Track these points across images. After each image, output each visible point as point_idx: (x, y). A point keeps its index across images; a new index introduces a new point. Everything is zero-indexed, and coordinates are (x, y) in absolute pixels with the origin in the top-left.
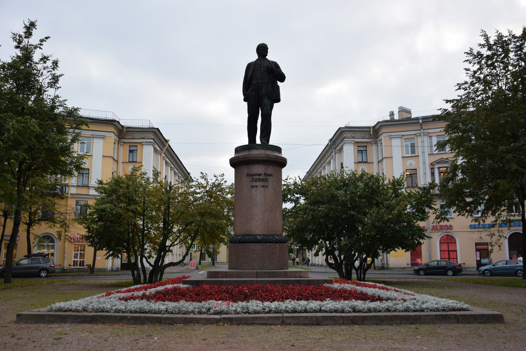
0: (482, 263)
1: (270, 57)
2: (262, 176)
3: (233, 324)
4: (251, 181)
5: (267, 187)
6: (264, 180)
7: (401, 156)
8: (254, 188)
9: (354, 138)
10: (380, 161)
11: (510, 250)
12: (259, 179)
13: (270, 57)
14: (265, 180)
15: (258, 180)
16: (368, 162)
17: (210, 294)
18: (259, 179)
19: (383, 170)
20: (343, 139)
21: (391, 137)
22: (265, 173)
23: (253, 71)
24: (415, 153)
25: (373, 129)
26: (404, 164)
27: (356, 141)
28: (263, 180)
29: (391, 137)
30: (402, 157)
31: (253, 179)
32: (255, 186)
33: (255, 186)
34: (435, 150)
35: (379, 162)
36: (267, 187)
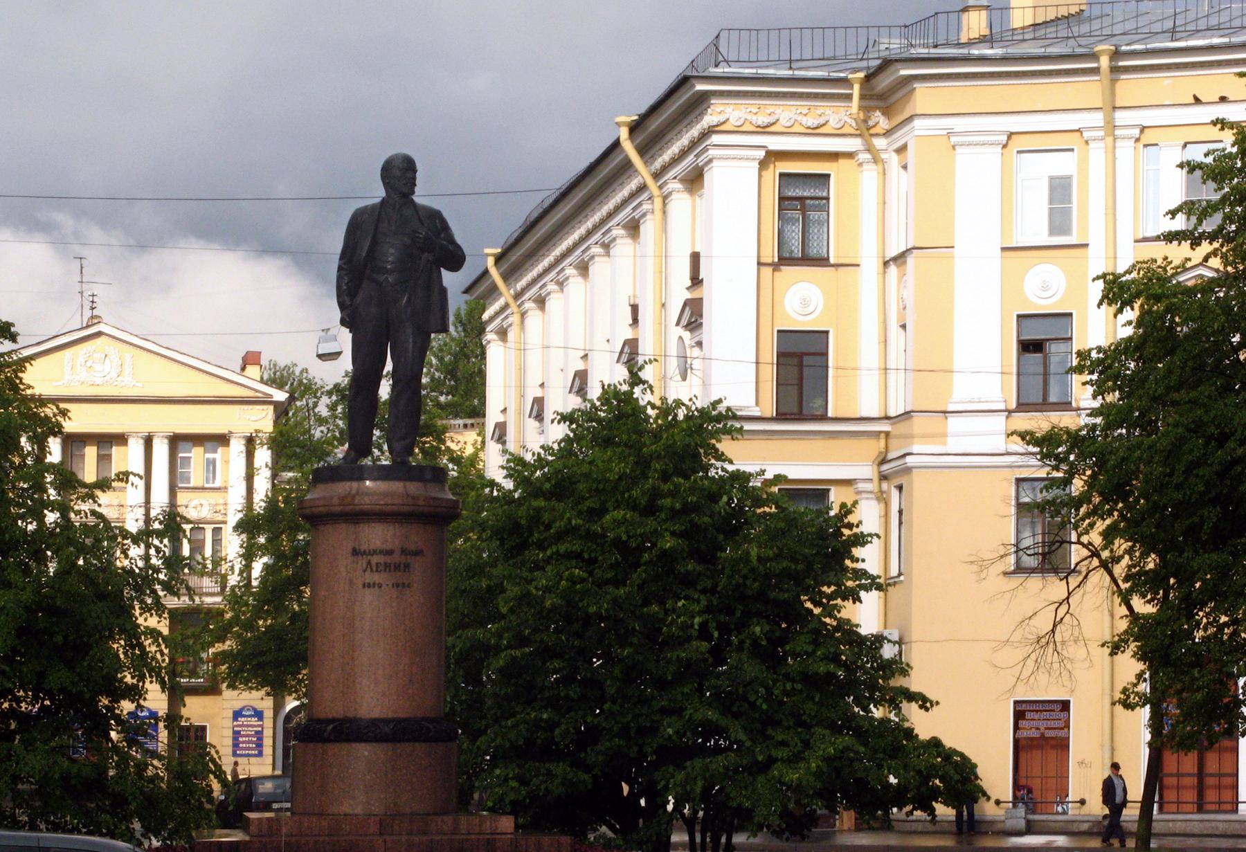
0: (272, 697)
1: (422, 196)
2: (394, 555)
3: (412, 814)
4: (365, 571)
5: (409, 586)
6: (399, 566)
7: (1000, 246)
8: (372, 590)
9: (763, 130)
10: (895, 259)
11: (1069, 738)
12: (385, 563)
13: (422, 196)
14: (402, 566)
15: (382, 568)
16: (832, 261)
17: (1106, 434)
18: (385, 563)
19: (905, 308)
20: (705, 135)
21: (954, 139)
22: (402, 548)
23: (375, 243)
24: (1066, 231)
25: (861, 89)
26: (1010, 285)
27: (772, 147)
28: (397, 567)
29: (954, 139)
30: (1004, 249)
31: (369, 563)
32: (374, 584)
33: (374, 584)
34: (1151, 233)
35: (886, 264)
36: (409, 586)
